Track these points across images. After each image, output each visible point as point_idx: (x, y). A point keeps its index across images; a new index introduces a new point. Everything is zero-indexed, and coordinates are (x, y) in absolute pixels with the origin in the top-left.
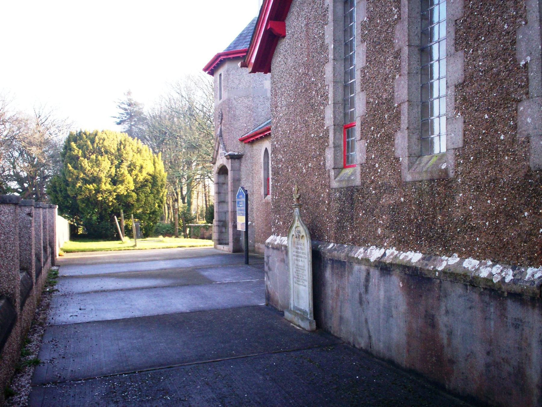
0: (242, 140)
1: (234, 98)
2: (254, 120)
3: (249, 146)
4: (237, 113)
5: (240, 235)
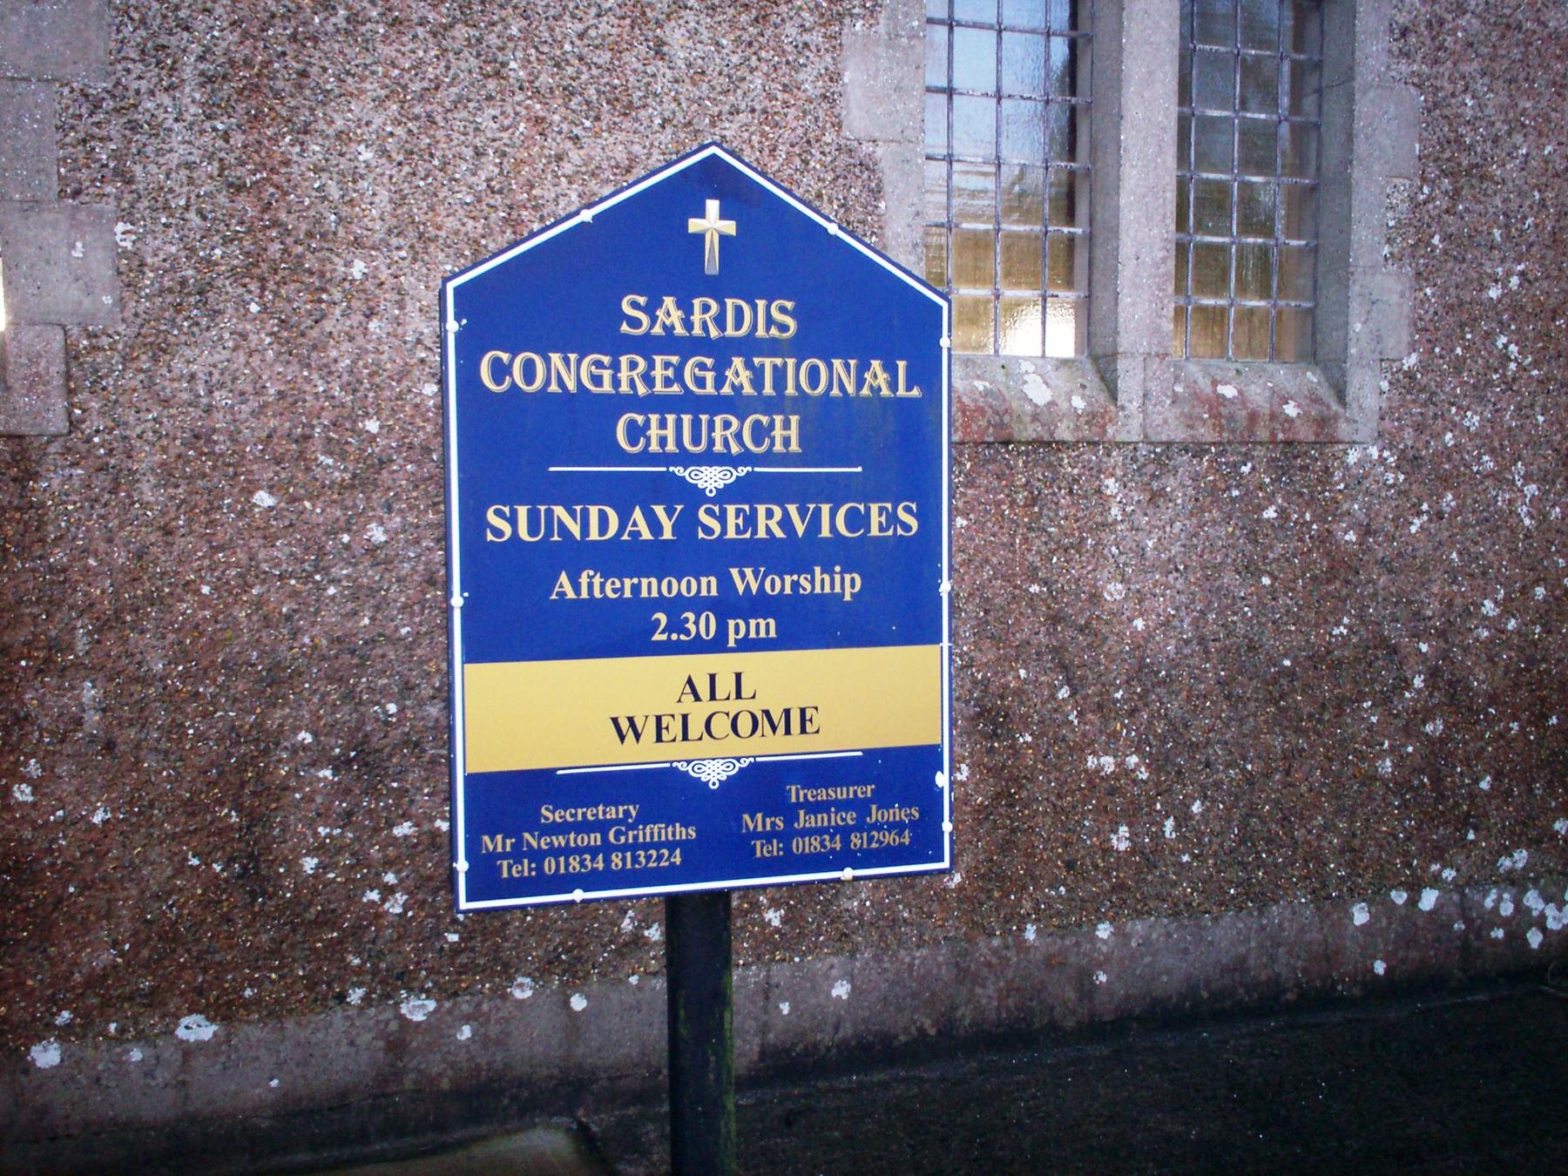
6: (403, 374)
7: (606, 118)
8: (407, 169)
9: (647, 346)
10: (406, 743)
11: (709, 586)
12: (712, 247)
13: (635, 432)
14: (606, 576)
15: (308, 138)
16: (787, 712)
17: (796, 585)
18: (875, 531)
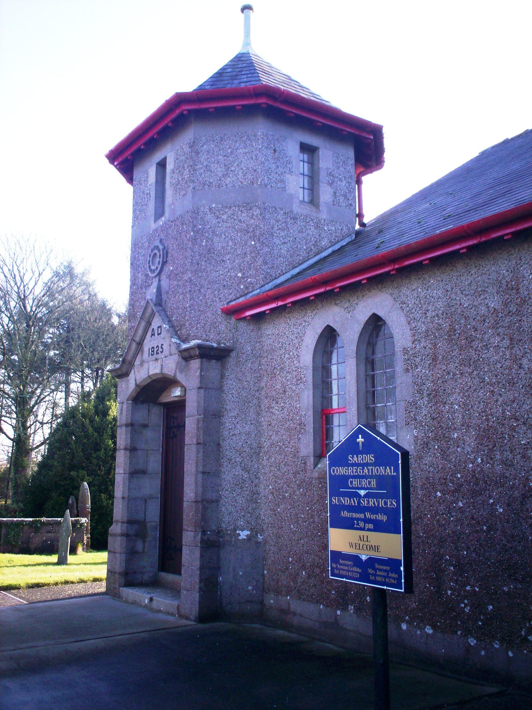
0: (230, 312)
1: (210, 209)
2: (265, 263)
3: (251, 327)
4: (218, 243)
5: (219, 568)
6: (465, 462)
7: (508, 388)
8: (464, 409)
9: (353, 465)
10: (468, 564)
11: (362, 516)
12: (361, 444)
13: (351, 482)
14: (348, 512)
15: (445, 405)
16: (375, 546)
17: (376, 517)
18: (389, 506)
